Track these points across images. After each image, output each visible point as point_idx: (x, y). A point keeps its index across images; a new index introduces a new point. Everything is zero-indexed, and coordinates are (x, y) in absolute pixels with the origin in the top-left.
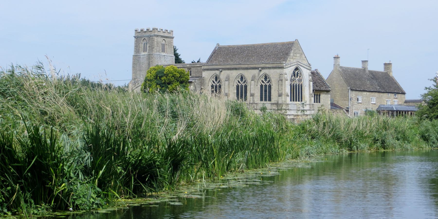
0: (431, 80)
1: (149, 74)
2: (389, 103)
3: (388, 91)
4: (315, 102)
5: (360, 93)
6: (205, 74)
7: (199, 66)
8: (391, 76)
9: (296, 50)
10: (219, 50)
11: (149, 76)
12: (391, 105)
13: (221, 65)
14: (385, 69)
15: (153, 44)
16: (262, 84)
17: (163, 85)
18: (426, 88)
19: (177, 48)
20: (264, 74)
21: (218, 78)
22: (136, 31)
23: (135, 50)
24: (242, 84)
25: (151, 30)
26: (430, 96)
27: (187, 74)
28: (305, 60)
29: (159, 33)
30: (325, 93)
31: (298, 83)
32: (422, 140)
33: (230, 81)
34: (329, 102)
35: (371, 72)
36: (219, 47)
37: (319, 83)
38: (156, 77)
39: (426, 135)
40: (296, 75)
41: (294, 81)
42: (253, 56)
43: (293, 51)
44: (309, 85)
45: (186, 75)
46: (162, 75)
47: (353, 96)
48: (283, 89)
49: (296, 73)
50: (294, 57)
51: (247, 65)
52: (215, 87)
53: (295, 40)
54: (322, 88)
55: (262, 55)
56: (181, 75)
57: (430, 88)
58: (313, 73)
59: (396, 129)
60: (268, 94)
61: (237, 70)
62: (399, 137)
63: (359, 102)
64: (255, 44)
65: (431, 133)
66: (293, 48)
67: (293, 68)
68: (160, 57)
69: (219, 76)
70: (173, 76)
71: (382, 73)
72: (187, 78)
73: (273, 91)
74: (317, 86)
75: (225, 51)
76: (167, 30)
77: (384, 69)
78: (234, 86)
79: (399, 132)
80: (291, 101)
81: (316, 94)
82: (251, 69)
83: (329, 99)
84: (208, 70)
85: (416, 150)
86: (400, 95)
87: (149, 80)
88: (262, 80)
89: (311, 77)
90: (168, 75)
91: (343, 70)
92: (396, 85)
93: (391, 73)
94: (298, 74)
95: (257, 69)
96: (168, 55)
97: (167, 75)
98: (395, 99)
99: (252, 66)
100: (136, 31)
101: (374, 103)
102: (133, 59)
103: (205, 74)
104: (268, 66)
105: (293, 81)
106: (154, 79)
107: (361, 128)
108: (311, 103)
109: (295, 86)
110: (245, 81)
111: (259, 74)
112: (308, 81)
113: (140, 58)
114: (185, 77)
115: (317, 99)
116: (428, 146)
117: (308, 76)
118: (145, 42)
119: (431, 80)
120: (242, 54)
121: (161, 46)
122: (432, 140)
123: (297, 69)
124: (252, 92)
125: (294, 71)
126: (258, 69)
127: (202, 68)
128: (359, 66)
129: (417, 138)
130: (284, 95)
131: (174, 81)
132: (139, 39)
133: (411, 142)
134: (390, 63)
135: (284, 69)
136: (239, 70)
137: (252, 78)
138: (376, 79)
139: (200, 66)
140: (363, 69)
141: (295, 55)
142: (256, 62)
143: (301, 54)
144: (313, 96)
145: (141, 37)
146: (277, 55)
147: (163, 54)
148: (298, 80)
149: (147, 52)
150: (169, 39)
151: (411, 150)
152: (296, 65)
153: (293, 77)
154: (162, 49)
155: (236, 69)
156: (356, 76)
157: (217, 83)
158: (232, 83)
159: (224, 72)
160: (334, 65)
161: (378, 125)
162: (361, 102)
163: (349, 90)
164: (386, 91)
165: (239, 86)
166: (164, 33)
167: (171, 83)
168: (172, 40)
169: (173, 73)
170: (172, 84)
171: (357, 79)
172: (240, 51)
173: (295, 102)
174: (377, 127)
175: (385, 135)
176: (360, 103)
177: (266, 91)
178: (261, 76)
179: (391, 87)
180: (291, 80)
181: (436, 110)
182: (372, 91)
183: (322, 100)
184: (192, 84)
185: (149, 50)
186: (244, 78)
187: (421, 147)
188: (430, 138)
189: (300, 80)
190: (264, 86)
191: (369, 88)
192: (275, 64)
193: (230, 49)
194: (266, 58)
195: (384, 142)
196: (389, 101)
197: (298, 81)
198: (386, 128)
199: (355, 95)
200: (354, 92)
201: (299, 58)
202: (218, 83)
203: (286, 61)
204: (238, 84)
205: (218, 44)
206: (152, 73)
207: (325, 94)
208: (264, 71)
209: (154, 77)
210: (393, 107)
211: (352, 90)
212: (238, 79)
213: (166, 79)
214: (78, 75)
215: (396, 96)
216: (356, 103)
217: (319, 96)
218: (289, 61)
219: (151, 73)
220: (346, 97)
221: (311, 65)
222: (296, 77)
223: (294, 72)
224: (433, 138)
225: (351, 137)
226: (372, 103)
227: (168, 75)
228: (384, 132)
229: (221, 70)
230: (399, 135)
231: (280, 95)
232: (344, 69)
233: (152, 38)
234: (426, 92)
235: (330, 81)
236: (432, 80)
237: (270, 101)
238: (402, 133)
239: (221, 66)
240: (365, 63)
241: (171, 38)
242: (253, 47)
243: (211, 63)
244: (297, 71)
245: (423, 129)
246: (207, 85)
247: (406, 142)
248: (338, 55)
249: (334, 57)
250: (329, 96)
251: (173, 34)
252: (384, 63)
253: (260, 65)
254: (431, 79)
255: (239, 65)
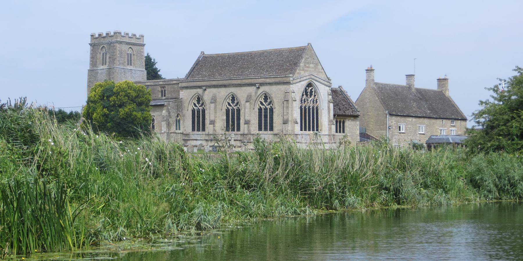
0: (489, 89)
1: (94, 92)
2: (444, 133)
3: (442, 116)
4: (337, 132)
5: (402, 119)
6: (184, 95)
7: (176, 84)
8: (447, 95)
9: (308, 58)
10: (204, 60)
11: (93, 95)
12: (446, 136)
13: (204, 81)
14: (439, 86)
15: (115, 54)
16: (260, 107)
17: (112, 108)
18: (482, 103)
19: (156, 61)
20: (264, 92)
21: (201, 99)
22: (92, 36)
23: (91, 63)
24: (233, 108)
25: (112, 34)
26: (487, 115)
27: (148, 93)
28: (322, 72)
29: (123, 38)
30: (352, 118)
31: (311, 105)
32: (470, 187)
33: (217, 104)
34: (358, 132)
35: (419, 91)
36: (203, 57)
37: (343, 105)
38: (102, 97)
39: (477, 178)
40: (309, 93)
41: (306, 102)
42: (249, 68)
43: (304, 59)
44: (329, 107)
45: (146, 94)
46: (110, 93)
47: (393, 124)
48: (290, 113)
49: (309, 91)
50: (305, 69)
51: (241, 80)
52: (197, 112)
53: (307, 45)
54: (348, 113)
55: (261, 67)
56: (139, 94)
57: (487, 102)
58: (334, 92)
59: (424, 168)
60: (269, 120)
61: (227, 87)
62: (429, 183)
63: (401, 131)
64: (252, 52)
65: (485, 175)
66: (305, 56)
67: (305, 83)
68: (124, 72)
69: (202, 97)
70: (126, 95)
71: (435, 92)
72: (147, 98)
73: (276, 116)
74: (340, 110)
75: (211, 62)
76: (127, 34)
77: (438, 86)
78: (223, 111)
79: (429, 174)
80: (301, 130)
81: (339, 121)
82: (246, 86)
83: (358, 127)
84: (187, 89)
85: (456, 206)
86: (459, 121)
87: (92, 102)
88: (260, 101)
89: (331, 97)
90: (119, 93)
91: (379, 88)
92: (453, 108)
93: (447, 92)
94: (311, 92)
95: (253, 86)
96: (136, 69)
97: (117, 94)
98: (453, 127)
99: (247, 81)
100: (92, 36)
101: (423, 133)
102: (89, 75)
103: (184, 95)
104: (268, 81)
105: (305, 101)
106: (99, 100)
107: (357, 167)
108: (331, 133)
109: (307, 110)
110: (237, 103)
111: (256, 93)
112: (327, 102)
113: (97, 73)
114: (145, 96)
115: (340, 127)
116: (480, 198)
117: (327, 95)
118: (104, 51)
119: (489, 89)
120: (234, 66)
121: (126, 57)
122: (488, 186)
123: (310, 85)
124: (247, 118)
125: (306, 88)
126: (255, 86)
127: (180, 85)
128: (403, 82)
129: (461, 183)
130: (291, 121)
131: (127, 102)
132: (96, 47)
133: (449, 190)
134: (446, 77)
135: (291, 86)
136: (229, 87)
137: (247, 98)
138: (426, 101)
139: (177, 83)
140: (408, 86)
141: (307, 65)
142: (252, 76)
143: (316, 64)
144: (335, 123)
145: (99, 45)
146: (283, 66)
147: (129, 67)
148: (312, 100)
149: (107, 65)
150: (138, 47)
151: (447, 205)
152: (309, 79)
153: (305, 96)
154: (128, 61)
155: (225, 86)
156: (397, 95)
157: (200, 107)
158: (220, 107)
159: (208, 90)
160: (366, 80)
161: (390, 162)
162: (403, 131)
163: (386, 115)
164: (439, 116)
165: (229, 110)
166: (130, 39)
167: (123, 105)
168: (142, 49)
169: (126, 91)
170: (126, 106)
171: (399, 100)
172: (232, 61)
173: (307, 132)
174: (388, 165)
175: (400, 180)
176: (403, 133)
177: (266, 116)
178: (260, 96)
179: (446, 111)
180: (301, 101)
181: (495, 137)
182: (420, 116)
183: (347, 128)
184: (165, 108)
185: (109, 63)
186: (235, 99)
187: (467, 199)
188: (484, 183)
189: (315, 101)
190: (264, 109)
191: (416, 112)
192: (278, 78)
193: (218, 59)
194: (266, 70)
195: (399, 191)
196: (444, 130)
197: (312, 102)
198: (404, 168)
199: (395, 121)
200: (394, 118)
201: (313, 70)
202: (201, 106)
203: (294, 74)
204: (228, 107)
205: (203, 53)
206: (97, 91)
207: (352, 121)
208: (263, 89)
209: (99, 98)
210: (448, 138)
211: (391, 115)
212: (228, 100)
213: (116, 99)
214: (23, 99)
215: (453, 124)
216: (397, 133)
217: (344, 123)
218: (299, 73)
219: (95, 91)
220: (383, 125)
221: (331, 80)
222: (309, 96)
223: (306, 90)
224: (489, 183)
225: (332, 184)
226: (419, 132)
227: (119, 93)
228: (400, 174)
229: (204, 88)
230: (429, 180)
231: (285, 122)
232: (381, 86)
233: (114, 46)
234: (482, 108)
235: (361, 103)
236: (491, 89)
237: (271, 131)
238: (434, 175)
239: (205, 82)
240: (410, 78)
241: (141, 46)
242: (249, 55)
243: (191, 79)
244: (310, 88)
245: (472, 168)
246: (187, 110)
247: (440, 191)
248: (371, 67)
249: (366, 70)
250: (358, 123)
251: (143, 40)
252: (438, 78)
253: (257, 79)
254: (489, 87)
255: (229, 81)
